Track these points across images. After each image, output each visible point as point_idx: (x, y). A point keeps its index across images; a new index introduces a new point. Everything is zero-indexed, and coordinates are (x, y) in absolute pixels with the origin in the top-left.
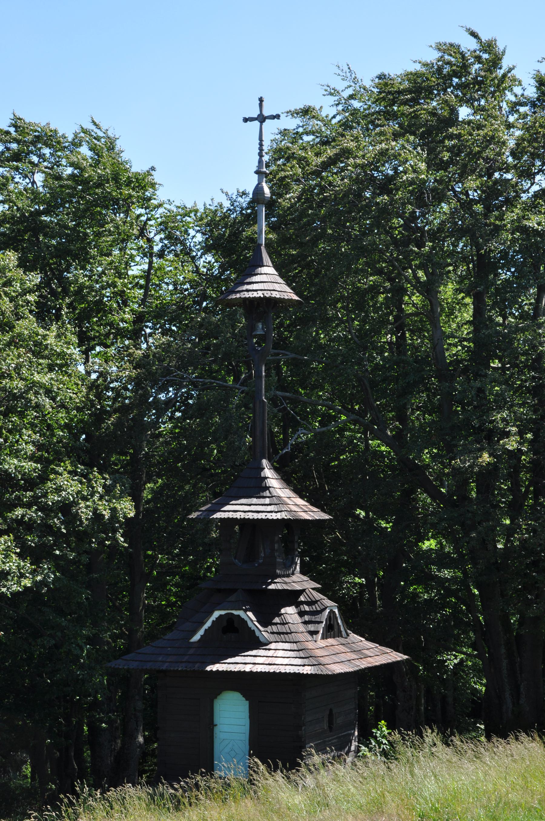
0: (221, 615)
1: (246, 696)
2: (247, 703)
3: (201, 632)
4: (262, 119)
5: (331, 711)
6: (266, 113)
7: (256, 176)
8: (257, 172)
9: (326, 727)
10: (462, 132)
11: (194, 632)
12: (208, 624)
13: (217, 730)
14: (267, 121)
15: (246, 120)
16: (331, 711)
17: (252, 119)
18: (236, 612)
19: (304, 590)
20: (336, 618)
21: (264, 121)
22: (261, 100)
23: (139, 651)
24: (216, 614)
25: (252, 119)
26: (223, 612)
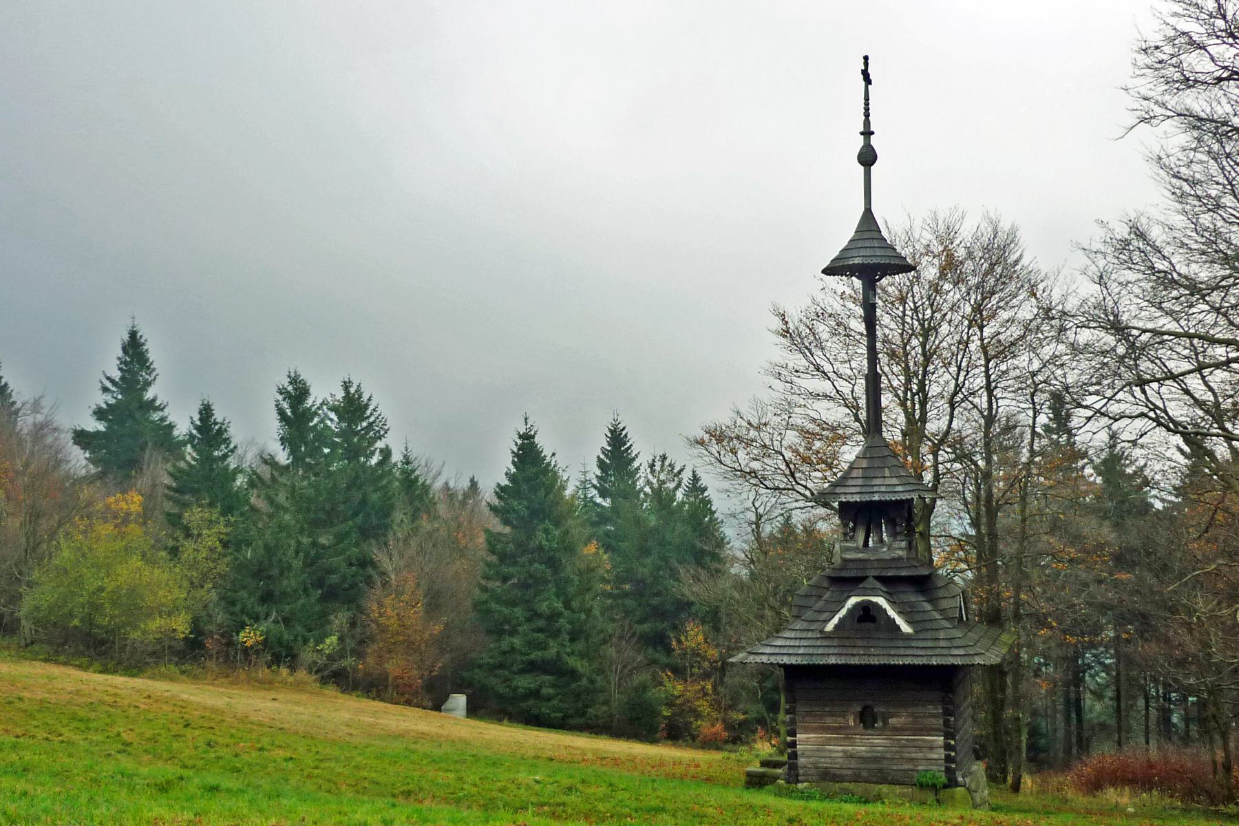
3: (835, 620)
8: (862, 133)
12: (843, 612)
18: (874, 599)
24: (853, 601)
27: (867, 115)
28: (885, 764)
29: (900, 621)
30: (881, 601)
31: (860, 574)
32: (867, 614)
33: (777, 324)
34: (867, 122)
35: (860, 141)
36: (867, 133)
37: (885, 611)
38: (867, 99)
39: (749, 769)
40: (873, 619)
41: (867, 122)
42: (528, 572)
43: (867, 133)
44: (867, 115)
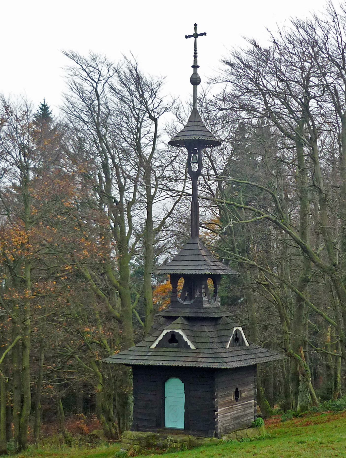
0: (168, 332)
1: (183, 381)
2: (183, 384)
3: (157, 342)
4: (196, 36)
5: (237, 389)
6: (198, 32)
7: (193, 69)
8: (192, 67)
9: (233, 398)
10: (23, 316)
11: (153, 342)
12: (161, 338)
13: (166, 400)
14: (199, 37)
15: (187, 37)
16: (237, 389)
17: (190, 36)
18: (176, 331)
19: (221, 317)
20: (241, 334)
21: (197, 37)
22: (196, 25)
23: (129, 349)
24: (165, 332)
25: (190, 36)
26: (169, 331)
27: (195, 56)
28: (156, 451)
29: (189, 343)
30: (180, 332)
31: (174, 315)
32: (173, 339)
33: (273, 39)
34: (195, 61)
35: (191, 71)
36: (195, 67)
37: (182, 337)
38: (195, 47)
39: (177, 344)
40: (176, 341)
41: (195, 61)
42: (42, 339)
43: (195, 67)
44: (195, 56)
